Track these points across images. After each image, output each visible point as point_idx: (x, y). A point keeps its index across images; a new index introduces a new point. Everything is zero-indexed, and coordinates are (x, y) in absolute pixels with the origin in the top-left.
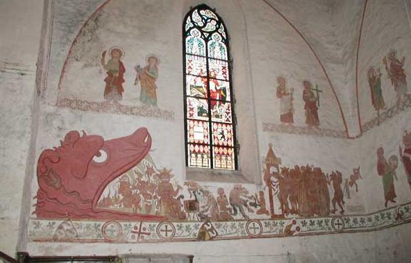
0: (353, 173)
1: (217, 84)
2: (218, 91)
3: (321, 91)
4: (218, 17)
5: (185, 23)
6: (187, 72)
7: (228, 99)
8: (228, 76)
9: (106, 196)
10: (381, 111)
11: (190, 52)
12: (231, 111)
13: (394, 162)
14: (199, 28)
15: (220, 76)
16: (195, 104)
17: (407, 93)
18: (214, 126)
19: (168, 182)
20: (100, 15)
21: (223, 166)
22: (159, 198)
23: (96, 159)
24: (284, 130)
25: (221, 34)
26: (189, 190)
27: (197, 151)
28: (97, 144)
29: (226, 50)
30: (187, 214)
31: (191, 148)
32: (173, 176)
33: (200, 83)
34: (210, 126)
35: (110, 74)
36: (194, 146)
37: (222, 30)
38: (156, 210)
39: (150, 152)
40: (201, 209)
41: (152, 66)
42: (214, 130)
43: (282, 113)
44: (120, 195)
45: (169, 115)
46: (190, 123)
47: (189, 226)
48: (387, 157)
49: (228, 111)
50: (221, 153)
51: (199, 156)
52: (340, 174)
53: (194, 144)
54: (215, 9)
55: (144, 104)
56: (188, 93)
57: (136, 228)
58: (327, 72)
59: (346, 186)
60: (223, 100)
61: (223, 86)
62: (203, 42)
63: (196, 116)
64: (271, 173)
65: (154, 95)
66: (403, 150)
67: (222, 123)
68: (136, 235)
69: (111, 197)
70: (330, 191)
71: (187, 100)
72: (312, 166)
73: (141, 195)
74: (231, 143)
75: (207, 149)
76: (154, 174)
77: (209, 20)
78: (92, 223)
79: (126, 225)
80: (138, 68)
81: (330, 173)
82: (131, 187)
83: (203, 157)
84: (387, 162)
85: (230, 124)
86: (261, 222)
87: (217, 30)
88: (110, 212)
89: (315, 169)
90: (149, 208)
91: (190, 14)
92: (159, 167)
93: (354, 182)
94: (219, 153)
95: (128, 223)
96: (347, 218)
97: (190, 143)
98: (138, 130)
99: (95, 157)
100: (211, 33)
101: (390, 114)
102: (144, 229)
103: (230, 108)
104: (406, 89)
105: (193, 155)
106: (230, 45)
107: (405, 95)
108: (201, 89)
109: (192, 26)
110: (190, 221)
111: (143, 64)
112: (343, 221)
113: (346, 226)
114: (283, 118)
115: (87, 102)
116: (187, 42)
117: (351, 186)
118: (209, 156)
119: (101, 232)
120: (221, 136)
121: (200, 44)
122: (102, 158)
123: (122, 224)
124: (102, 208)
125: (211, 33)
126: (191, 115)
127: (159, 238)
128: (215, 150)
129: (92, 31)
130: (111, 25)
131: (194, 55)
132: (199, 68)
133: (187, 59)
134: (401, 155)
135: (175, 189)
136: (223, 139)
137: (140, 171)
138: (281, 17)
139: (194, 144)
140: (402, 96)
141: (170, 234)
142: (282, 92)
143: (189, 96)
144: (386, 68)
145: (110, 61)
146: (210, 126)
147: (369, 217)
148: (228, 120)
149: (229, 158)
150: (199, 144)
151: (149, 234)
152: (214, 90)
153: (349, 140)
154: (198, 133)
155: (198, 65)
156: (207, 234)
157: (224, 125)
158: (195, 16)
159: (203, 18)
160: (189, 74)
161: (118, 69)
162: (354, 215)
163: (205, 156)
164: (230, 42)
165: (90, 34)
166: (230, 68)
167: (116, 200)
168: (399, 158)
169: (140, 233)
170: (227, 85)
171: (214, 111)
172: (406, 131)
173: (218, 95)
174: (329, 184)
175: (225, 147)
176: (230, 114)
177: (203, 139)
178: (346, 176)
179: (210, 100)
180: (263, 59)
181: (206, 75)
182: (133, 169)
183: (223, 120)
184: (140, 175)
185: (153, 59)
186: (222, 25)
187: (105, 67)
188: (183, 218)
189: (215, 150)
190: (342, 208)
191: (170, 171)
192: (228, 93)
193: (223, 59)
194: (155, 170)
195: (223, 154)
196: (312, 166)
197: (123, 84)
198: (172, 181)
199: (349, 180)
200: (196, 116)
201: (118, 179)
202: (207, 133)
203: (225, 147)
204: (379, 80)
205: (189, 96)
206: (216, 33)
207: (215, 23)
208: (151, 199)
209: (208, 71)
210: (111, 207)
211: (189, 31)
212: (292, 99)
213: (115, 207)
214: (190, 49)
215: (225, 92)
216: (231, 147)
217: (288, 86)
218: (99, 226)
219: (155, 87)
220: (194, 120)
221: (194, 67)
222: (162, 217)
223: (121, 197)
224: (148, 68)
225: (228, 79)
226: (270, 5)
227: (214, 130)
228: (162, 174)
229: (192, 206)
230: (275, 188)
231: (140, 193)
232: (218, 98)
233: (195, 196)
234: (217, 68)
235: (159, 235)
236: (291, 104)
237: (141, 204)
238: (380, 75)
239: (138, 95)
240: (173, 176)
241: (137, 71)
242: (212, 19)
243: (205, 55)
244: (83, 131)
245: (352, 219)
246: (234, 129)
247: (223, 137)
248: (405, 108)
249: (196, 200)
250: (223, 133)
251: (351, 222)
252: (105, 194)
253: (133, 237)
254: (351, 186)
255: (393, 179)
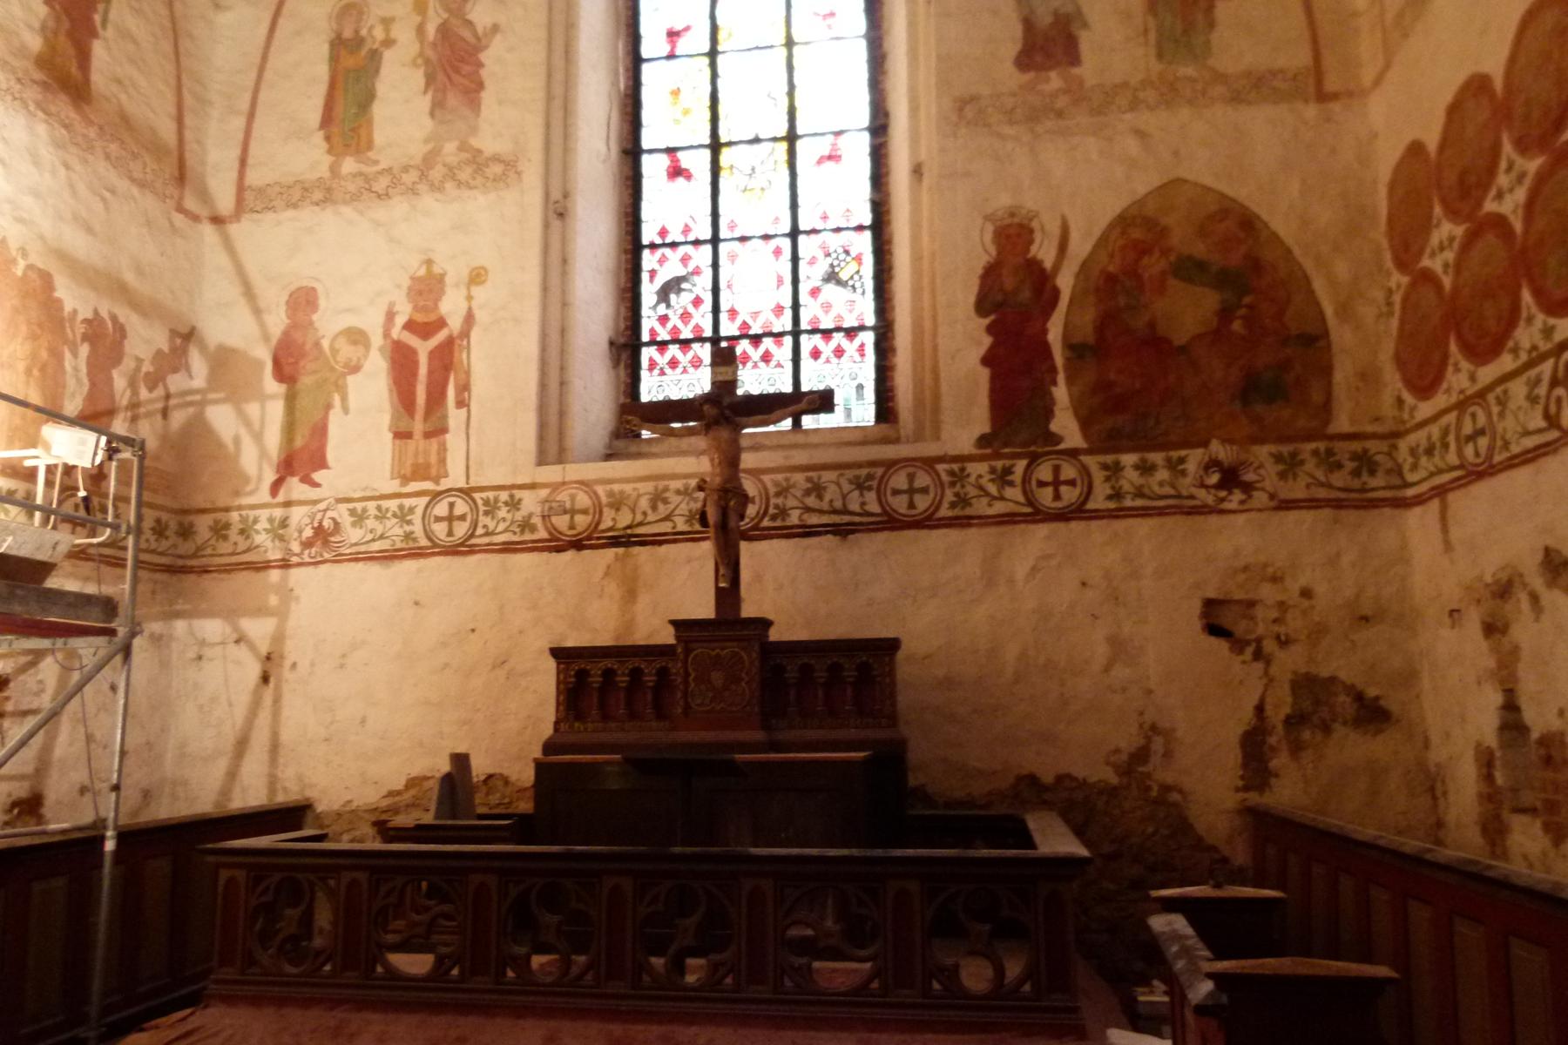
10: (349, 165)
13: (347, 351)
17: (475, 142)
24: (1170, 93)
48: (328, 324)
52: (121, 331)
66: (400, 321)
84: (325, 344)
86: (477, 496)
93: (163, 379)
101: (370, 191)
104: (474, 130)
107: (463, 147)
134: (386, 334)
140: (450, 147)
144: (420, 30)
153: (179, 219)
168: (377, 340)
172: (429, 262)
199: (147, 367)
204: (375, 57)
238: (389, 43)
248: (449, 185)
255: (329, 407)
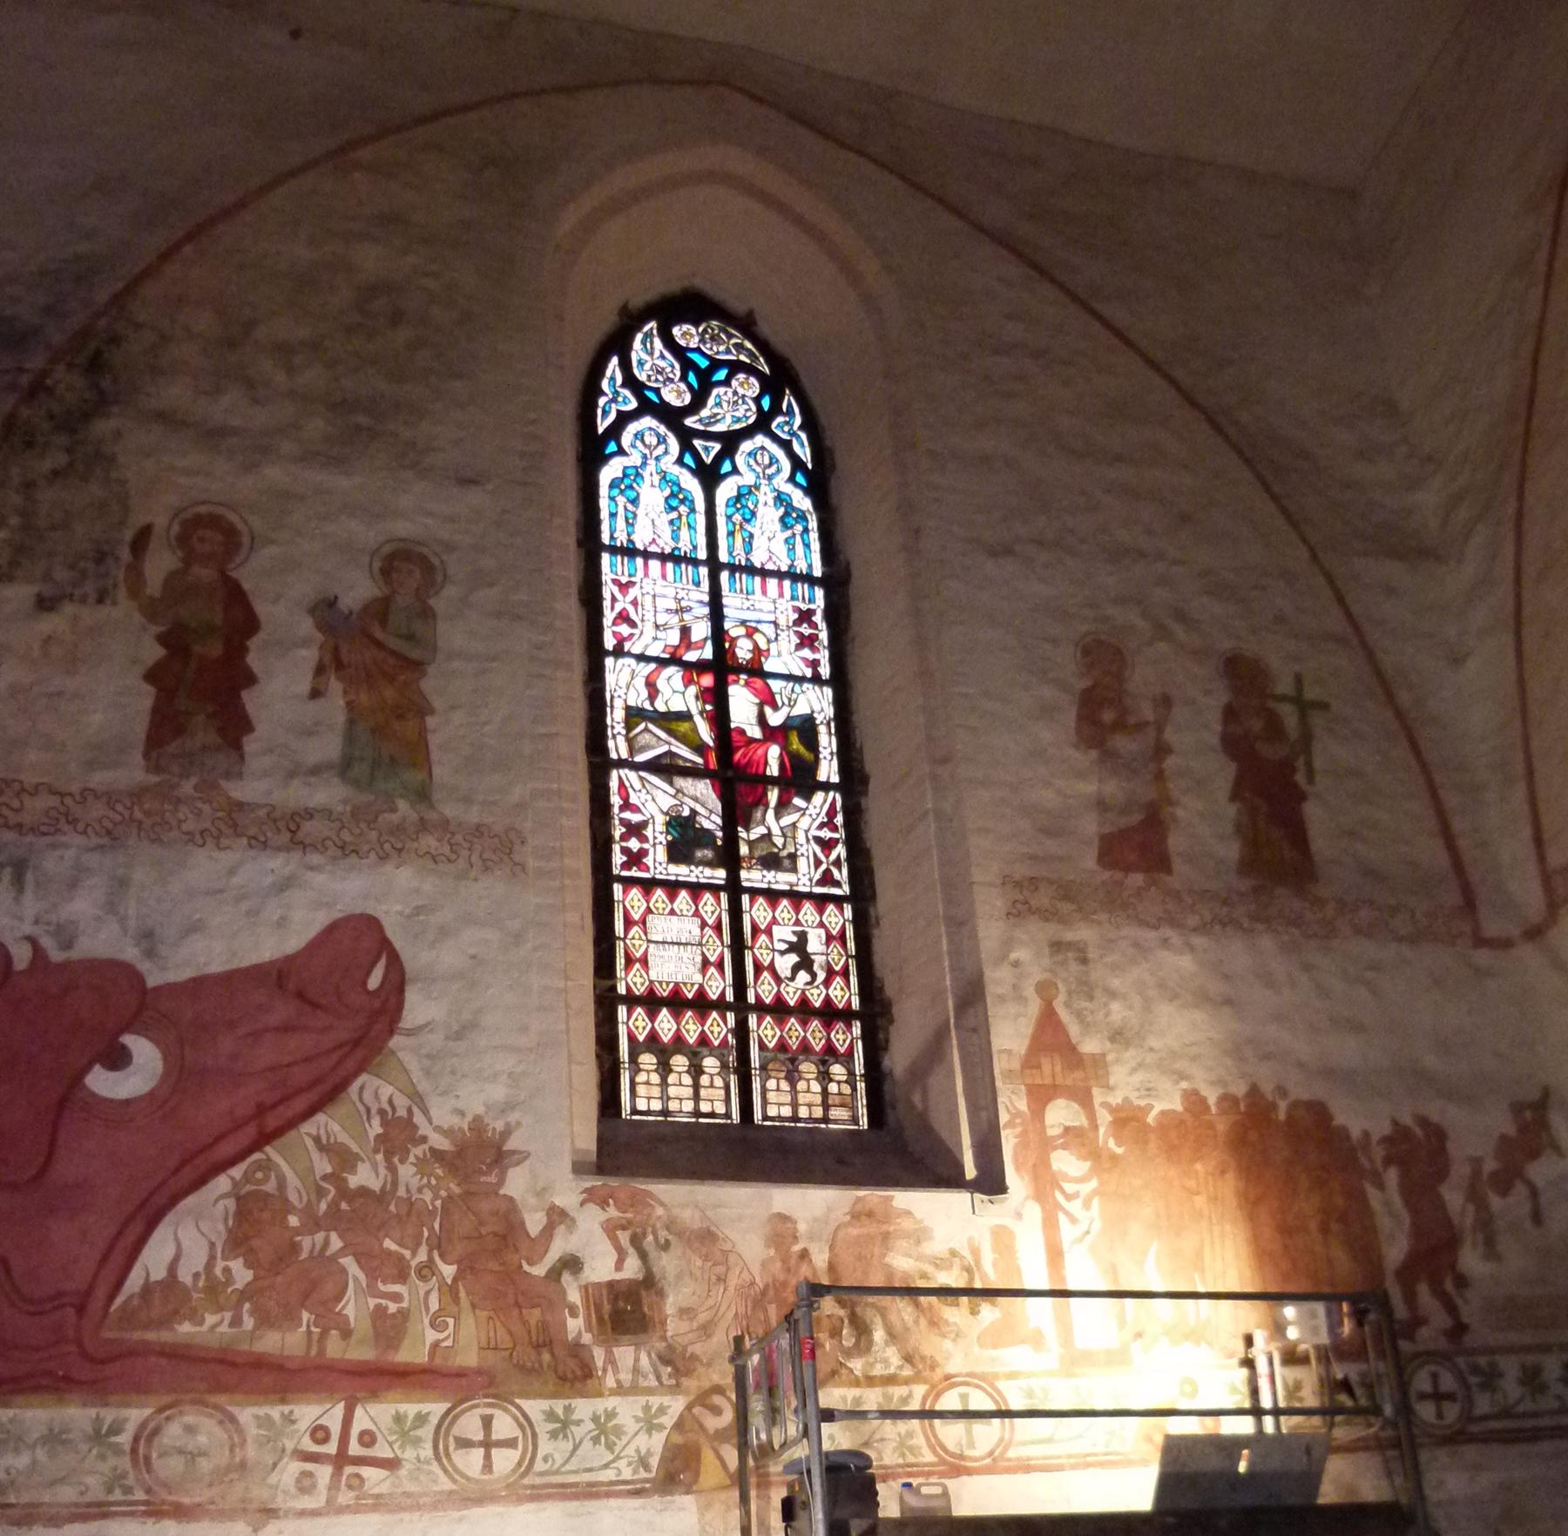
0: (1510, 1130)
1: (768, 699)
2: (771, 734)
3: (1323, 706)
4: (764, 347)
5: (591, 390)
6: (609, 643)
7: (828, 770)
8: (824, 656)
9: (159, 1274)
11: (621, 538)
12: (840, 834)
14: (671, 417)
15: (784, 658)
16: (651, 802)
18: (756, 912)
19: (493, 1191)
20: (115, 340)
21: (803, 1112)
22: (448, 1271)
23: (100, 1082)
25: (786, 446)
26: (611, 1229)
27: (666, 1037)
28: (110, 1003)
29: (813, 524)
30: (599, 1355)
31: (634, 1023)
32: (521, 1157)
33: (677, 694)
34: (736, 912)
35: (176, 641)
36: (652, 1016)
37: (790, 423)
38: (431, 1336)
39: (395, 1042)
40: (673, 1327)
41: (404, 600)
42: (755, 930)
43: (1107, 830)
44: (237, 1265)
45: (498, 849)
46: (630, 901)
47: (611, 1415)
49: (826, 834)
50: (794, 1044)
51: (680, 1062)
53: (651, 1002)
54: (751, 314)
55: (366, 798)
56: (617, 747)
57: (320, 1433)
58: (1356, 609)
59: (1474, 1195)
60: (799, 778)
61: (801, 709)
62: (692, 485)
63: (658, 863)
64: (1053, 1132)
65: (417, 753)
67: (796, 898)
68: (324, 1473)
69: (185, 1276)
70: (1384, 1223)
71: (614, 784)
72: (1282, 1091)
73: (349, 1262)
74: (845, 994)
75: (719, 1027)
76: (418, 1151)
77: (721, 375)
78: (77, 1415)
79: (551, 1416)
80: (325, 610)
81: (1383, 1128)
82: (293, 1221)
83: (696, 1071)
85: (838, 901)
87: (762, 424)
88: (181, 1355)
89: (1295, 1105)
90: (389, 1328)
91: (618, 342)
92: (442, 1119)
94: (782, 1046)
95: (275, 1412)
96: (1482, 1361)
97: (631, 1000)
98: (332, 929)
99: (97, 1068)
100: (730, 442)
102: (368, 1439)
103: (839, 820)
105: (648, 1060)
106: (834, 499)
108: (684, 727)
109: (633, 404)
110: (620, 1390)
111: (357, 590)
112: (1460, 1377)
113: (1483, 1404)
114: (1113, 851)
115: (53, 792)
116: (604, 491)
117: (1504, 1192)
118: (732, 1059)
119: (125, 1463)
120: (793, 958)
121: (676, 498)
122: (142, 1070)
123: (247, 1415)
124: (137, 1335)
125: (730, 442)
126: (635, 859)
127: (445, 1484)
128: (764, 1031)
129: (73, 422)
130: (175, 393)
131: (647, 555)
132: (674, 620)
133: (607, 575)
135: (534, 1223)
136: (803, 976)
137: (343, 1138)
138: (1096, 326)
139: (651, 1002)
141: (504, 1460)
142: (1108, 716)
143: (621, 763)
145: (172, 577)
146: (736, 912)
147: (1530, 1359)
148: (827, 879)
149: (837, 1070)
150: (676, 1002)
151: (391, 1464)
152: (755, 732)
153: (1483, 957)
154: (672, 944)
155: (663, 604)
156: (708, 1456)
157: (808, 907)
158: (648, 355)
159: (687, 366)
160: (619, 652)
161: (218, 618)
162: (1528, 1349)
163: (711, 1064)
164: (833, 483)
165: (62, 439)
166: (837, 615)
167: (214, 1289)
169: (341, 1459)
170: (817, 702)
171: (757, 832)
173: (774, 751)
174: (1381, 1186)
175: (816, 1013)
176: (840, 851)
177: (698, 978)
178: (1475, 1134)
179: (738, 784)
180: (1008, 551)
181: (708, 653)
182: (308, 1128)
183: (804, 878)
184: (345, 1160)
185: (407, 566)
186: (788, 400)
187: (151, 610)
188: (576, 1375)
189: (764, 1031)
190: (1452, 1309)
191: (507, 1133)
192: (827, 742)
193: (801, 566)
194: (424, 1129)
195: (805, 1047)
196: (1282, 1091)
197: (245, 695)
198: (516, 1184)
199: (1490, 1165)
200: (658, 863)
201: (222, 1183)
202: (718, 948)
203: (816, 1013)
205: (621, 763)
206: (760, 440)
207: (754, 387)
208: (402, 1277)
209: (719, 634)
210: (186, 1328)
211: (615, 430)
212: (1161, 750)
213: (209, 1328)
214: (621, 523)
215: (811, 742)
216: (847, 1015)
217: (1142, 678)
218: (116, 1429)
219: (422, 710)
220: (648, 886)
221: (646, 617)
222: (461, 1374)
223: (242, 1275)
224: (380, 610)
225: (825, 671)
226: (1034, 266)
227: (755, 930)
228: (461, 1152)
229: (626, 1311)
230: (1075, 1207)
231: (342, 1252)
232: (773, 770)
233: (643, 1256)
234: (771, 619)
235: (451, 1472)
236: (1159, 776)
237: (352, 1308)
239: (329, 747)
240: (521, 1157)
241: (322, 626)
242: (735, 367)
243: (702, 554)
244: (33, 941)
245: (1510, 1367)
246: (862, 922)
247: (805, 963)
249: (649, 1281)
250: (799, 945)
251: (1511, 1387)
252: (154, 1260)
253: (305, 1484)
254: (1504, 1192)
